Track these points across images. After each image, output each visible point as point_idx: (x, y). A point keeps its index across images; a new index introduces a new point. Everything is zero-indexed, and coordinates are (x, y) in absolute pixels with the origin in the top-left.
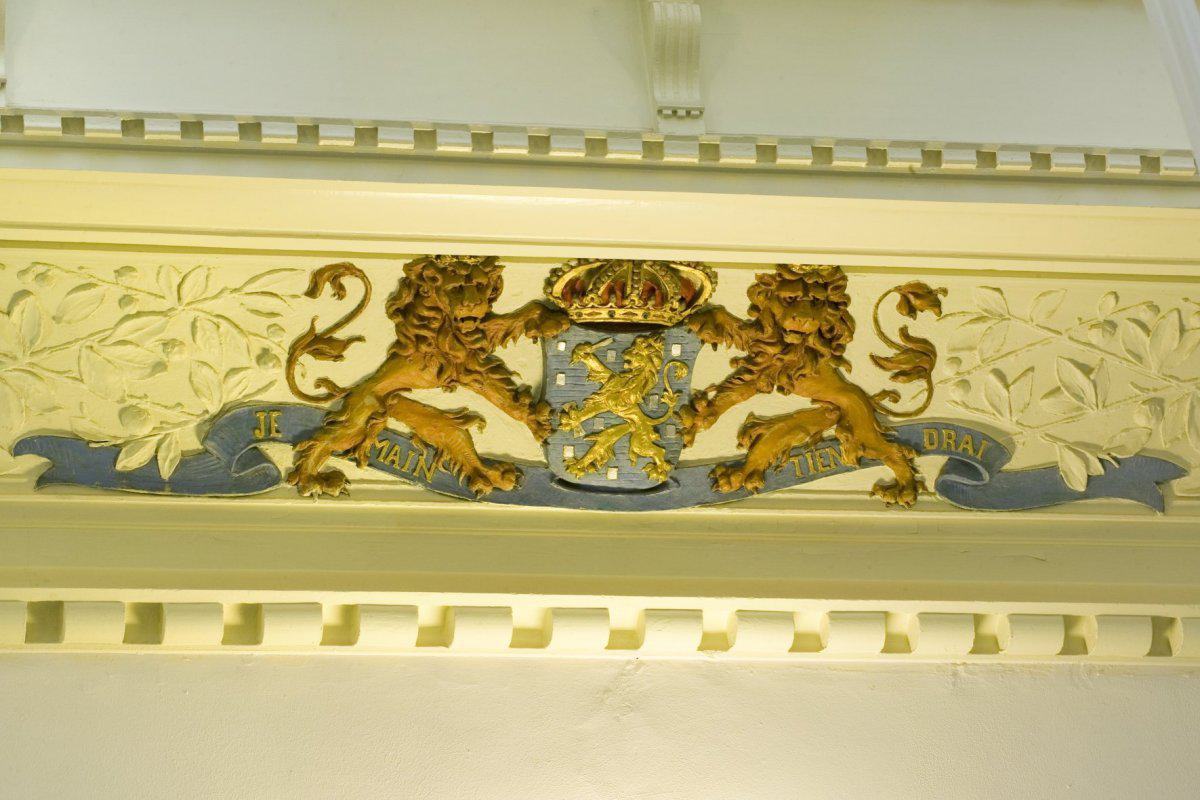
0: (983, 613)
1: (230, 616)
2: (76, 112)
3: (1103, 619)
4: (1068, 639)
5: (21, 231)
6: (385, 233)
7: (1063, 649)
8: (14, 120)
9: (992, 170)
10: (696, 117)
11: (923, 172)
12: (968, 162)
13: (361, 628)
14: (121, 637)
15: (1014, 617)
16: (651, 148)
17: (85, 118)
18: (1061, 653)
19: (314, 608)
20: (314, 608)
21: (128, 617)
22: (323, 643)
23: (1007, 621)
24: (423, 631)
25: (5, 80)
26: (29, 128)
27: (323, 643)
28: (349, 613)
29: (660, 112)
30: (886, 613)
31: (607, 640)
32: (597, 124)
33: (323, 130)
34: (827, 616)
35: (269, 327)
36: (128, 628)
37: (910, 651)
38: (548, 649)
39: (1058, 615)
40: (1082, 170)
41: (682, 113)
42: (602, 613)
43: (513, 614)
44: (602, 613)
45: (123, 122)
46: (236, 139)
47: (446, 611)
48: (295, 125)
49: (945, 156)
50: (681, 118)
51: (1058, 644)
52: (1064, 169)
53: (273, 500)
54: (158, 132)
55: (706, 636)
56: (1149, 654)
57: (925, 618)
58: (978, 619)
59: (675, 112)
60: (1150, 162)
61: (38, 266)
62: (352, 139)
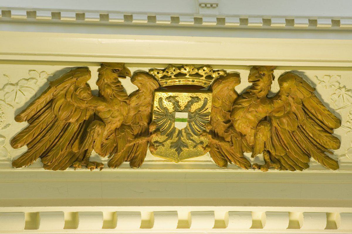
0: (330, 212)
1: (67, 217)
2: (8, 8)
3: (343, 215)
4: (328, 222)
5: (180, 60)
6: (144, 56)
7: (251, 227)
8: (6, 12)
9: (338, 27)
10: (214, 8)
11: (195, 26)
12: (305, 24)
13: (41, 221)
14: (63, 226)
15: (231, 213)
16: (198, 20)
17: (61, 12)
18: (288, 228)
19: (61, 214)
20: (61, 214)
21: (27, 218)
22: (103, 228)
23: (340, 216)
24: (105, 222)
25: (218, 4)
26: (38, 16)
27: (103, 228)
28: (74, 215)
29: (200, 5)
30: (289, 213)
31: (214, 225)
32: (175, 10)
33: (87, 15)
34: (265, 214)
35: (206, 98)
36: (27, 223)
37: (262, 228)
38: (116, 229)
39: (325, 213)
40: (75, 19)
41: (209, 5)
42: (212, 213)
43: (142, 215)
44: (212, 213)
45: (148, 17)
46: (75, 19)
47: (114, 214)
48: (123, 15)
49: (250, 21)
50: (208, 7)
51: (325, 224)
52: (68, 19)
53: (143, 169)
54: (42, 16)
55: (216, 221)
56: (326, 229)
57: (343, 215)
58: (328, 215)
59: (206, 5)
60: (336, 22)
61: (31, 72)
62: (215, 22)
